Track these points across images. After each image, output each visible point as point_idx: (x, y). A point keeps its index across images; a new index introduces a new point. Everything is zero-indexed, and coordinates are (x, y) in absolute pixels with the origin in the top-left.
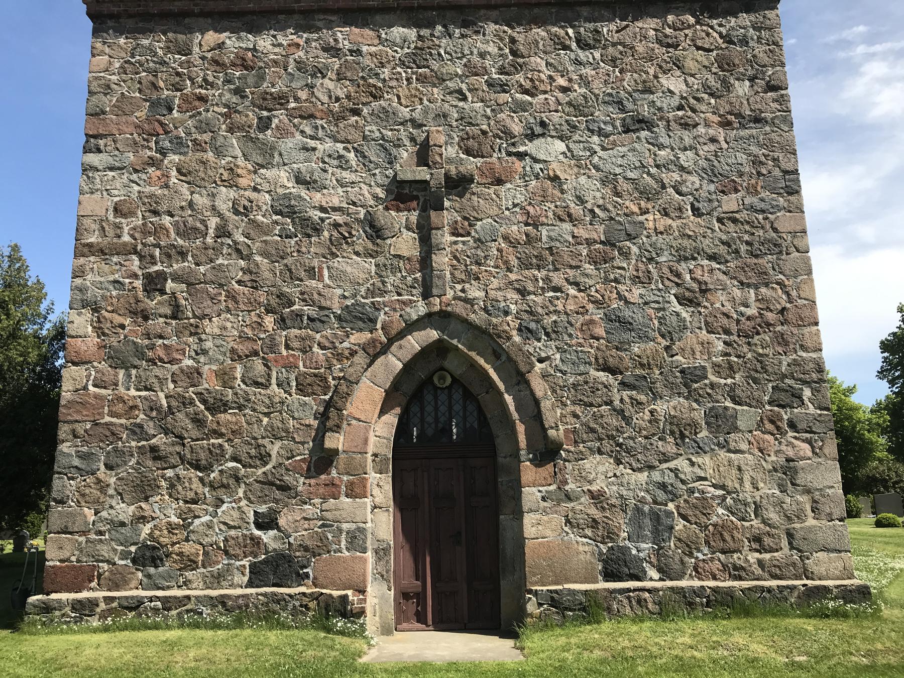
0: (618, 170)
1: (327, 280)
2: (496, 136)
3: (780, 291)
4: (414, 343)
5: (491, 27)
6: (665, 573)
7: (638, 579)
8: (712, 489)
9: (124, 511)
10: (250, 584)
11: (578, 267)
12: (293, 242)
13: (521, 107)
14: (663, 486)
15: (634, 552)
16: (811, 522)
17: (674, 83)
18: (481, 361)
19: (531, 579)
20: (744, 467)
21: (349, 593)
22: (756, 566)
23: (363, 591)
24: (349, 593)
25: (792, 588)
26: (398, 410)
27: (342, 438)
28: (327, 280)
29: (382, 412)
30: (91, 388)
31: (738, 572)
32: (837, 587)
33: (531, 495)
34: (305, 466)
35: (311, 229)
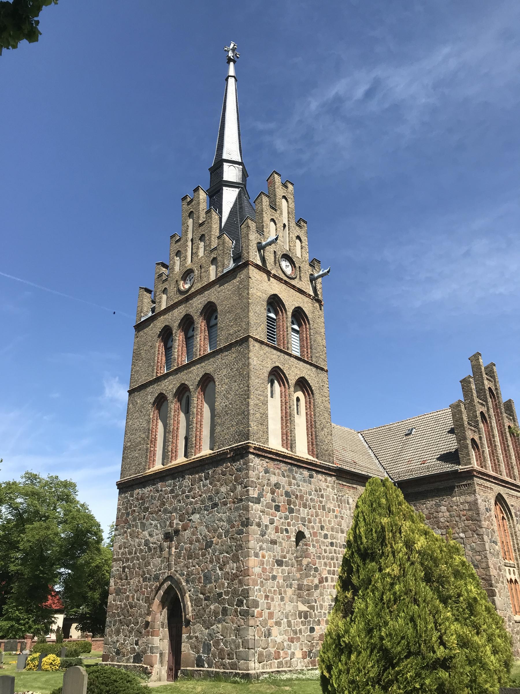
0: (209, 523)
1: (152, 567)
2: (186, 514)
3: (241, 564)
4: (165, 586)
5: (187, 476)
6: (210, 666)
7: (203, 667)
8: (220, 636)
9: (115, 638)
10: (133, 663)
11: (199, 558)
12: (427, 526)
13: (191, 503)
14: (210, 635)
15: (203, 658)
16: (241, 649)
17: (223, 489)
18: (178, 592)
19: (182, 665)
20: (228, 629)
21: (148, 666)
22: (228, 665)
23: (152, 666)
24: (148, 666)
25: (232, 672)
26: (167, 608)
27: (150, 617)
28: (152, 567)
29: (163, 609)
30: (112, 602)
31: (224, 666)
32: (242, 673)
33: (184, 636)
34: (144, 626)
35: (150, 549)
